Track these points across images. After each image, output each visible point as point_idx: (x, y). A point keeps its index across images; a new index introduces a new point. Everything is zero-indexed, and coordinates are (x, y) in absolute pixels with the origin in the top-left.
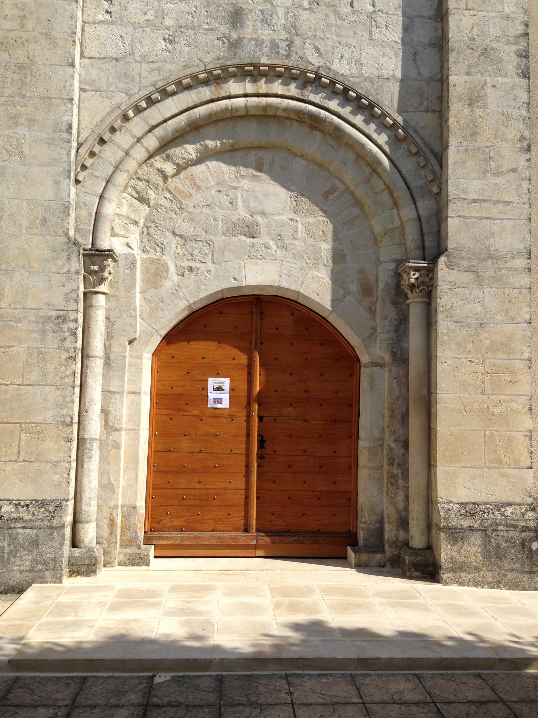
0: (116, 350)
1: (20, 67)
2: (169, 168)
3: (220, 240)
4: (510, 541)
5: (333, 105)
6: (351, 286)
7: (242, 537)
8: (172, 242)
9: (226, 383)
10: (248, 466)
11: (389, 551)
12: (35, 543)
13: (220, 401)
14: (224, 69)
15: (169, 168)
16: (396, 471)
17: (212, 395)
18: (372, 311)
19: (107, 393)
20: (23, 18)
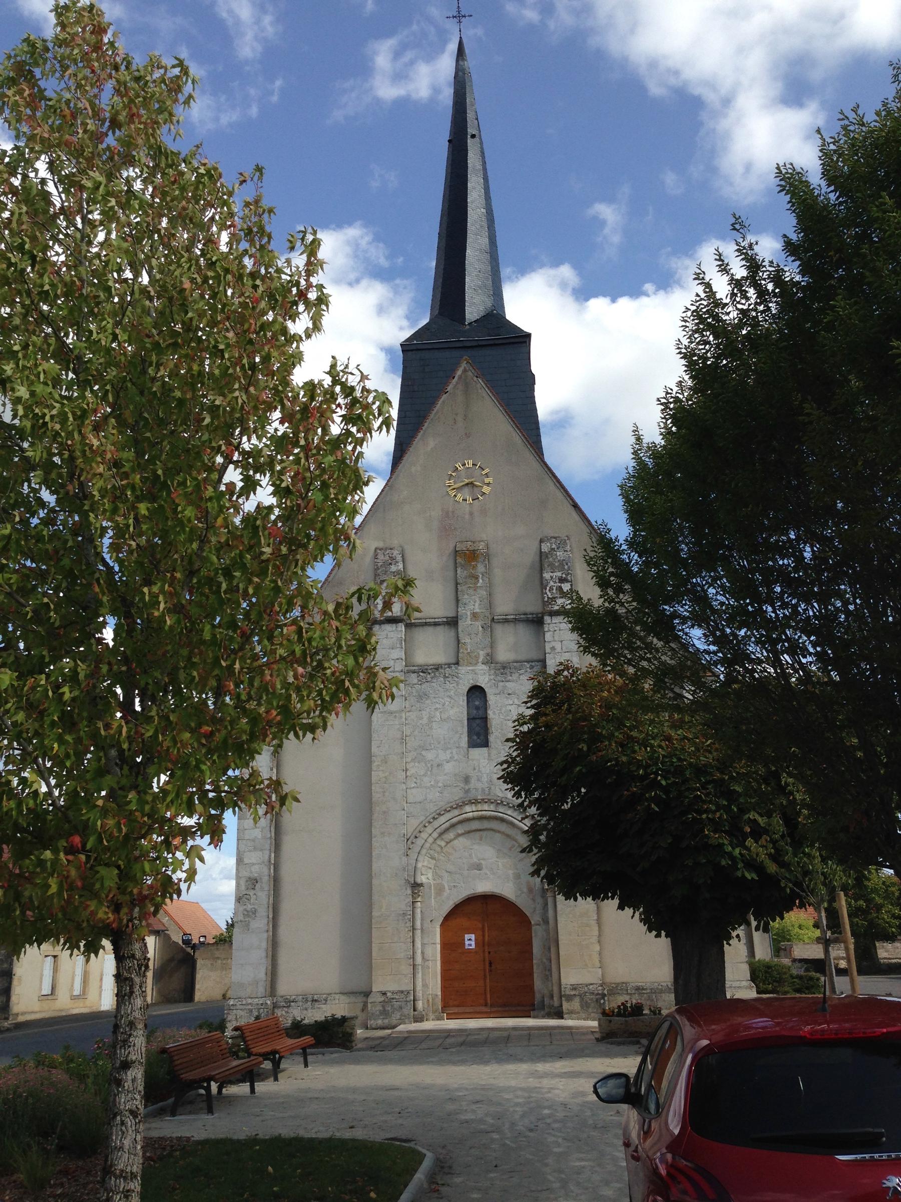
0: (426, 925)
1: (385, 812)
2: (443, 844)
3: (466, 872)
4: (591, 999)
5: (509, 812)
6: (714, 591)
7: (484, 1009)
8: (446, 875)
9: (473, 937)
10: (485, 975)
11: (547, 1010)
12: (401, 1008)
13: (470, 945)
14: (463, 802)
15: (443, 844)
16: (547, 973)
17: (467, 943)
18: (534, 900)
19: (423, 945)
20: (384, 792)
